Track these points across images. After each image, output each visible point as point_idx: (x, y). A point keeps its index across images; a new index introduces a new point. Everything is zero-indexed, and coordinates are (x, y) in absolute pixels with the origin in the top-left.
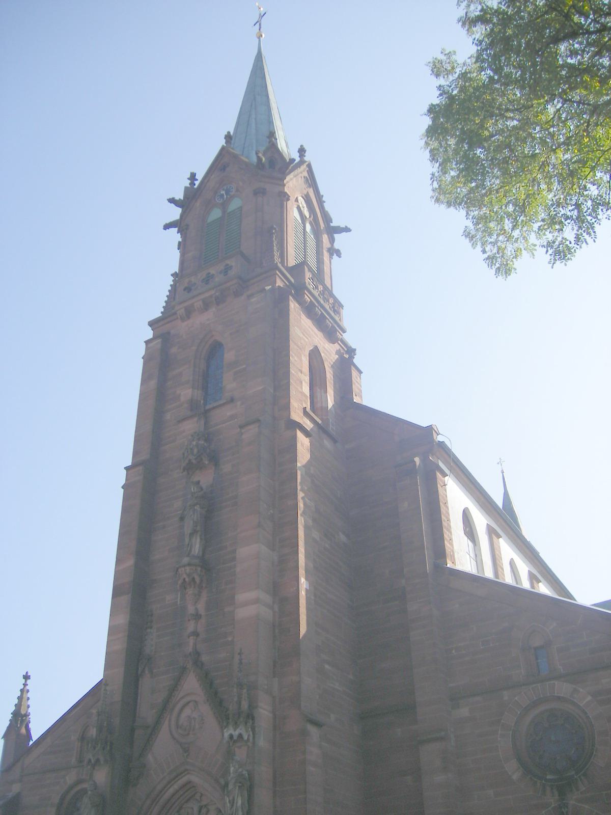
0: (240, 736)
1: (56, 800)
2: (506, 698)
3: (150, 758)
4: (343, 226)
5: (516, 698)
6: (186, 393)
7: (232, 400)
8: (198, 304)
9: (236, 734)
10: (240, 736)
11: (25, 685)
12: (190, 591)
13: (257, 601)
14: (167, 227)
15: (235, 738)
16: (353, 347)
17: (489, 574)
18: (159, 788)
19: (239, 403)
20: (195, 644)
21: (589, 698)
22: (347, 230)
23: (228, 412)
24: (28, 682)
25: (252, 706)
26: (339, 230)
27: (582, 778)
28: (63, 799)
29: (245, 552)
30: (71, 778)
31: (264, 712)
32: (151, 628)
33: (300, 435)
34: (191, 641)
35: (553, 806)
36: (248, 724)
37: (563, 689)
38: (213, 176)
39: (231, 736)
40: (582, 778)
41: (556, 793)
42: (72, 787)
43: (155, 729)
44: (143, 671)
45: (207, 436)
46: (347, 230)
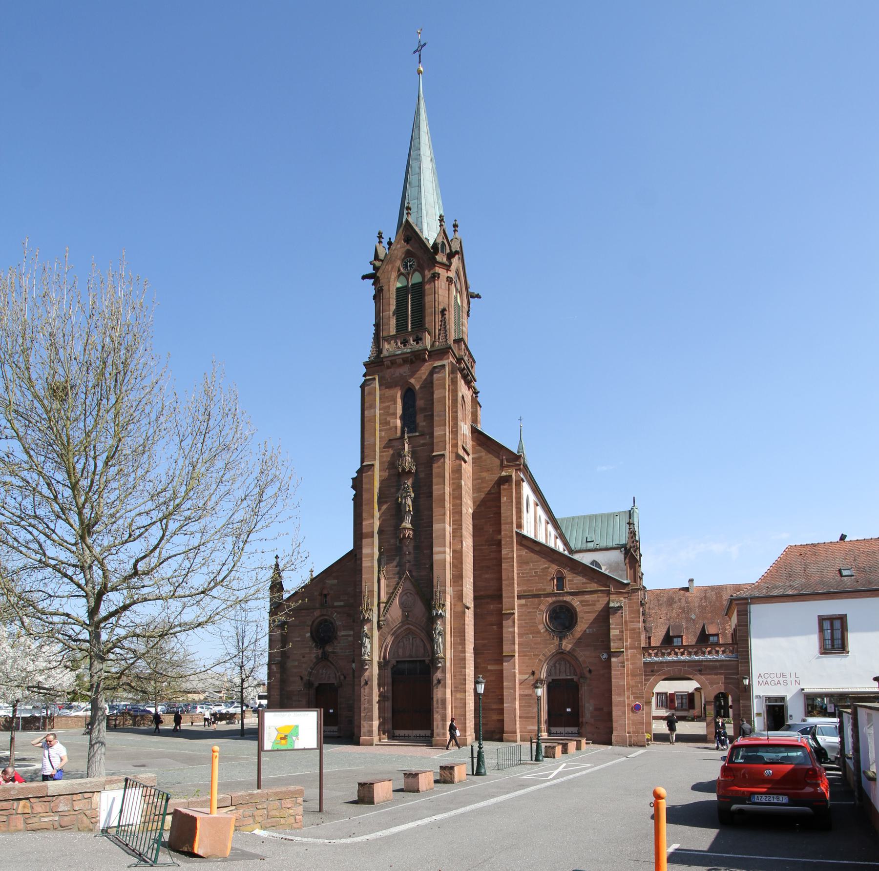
1: (310, 623)
30: (317, 613)
37: (568, 598)
42: (317, 618)
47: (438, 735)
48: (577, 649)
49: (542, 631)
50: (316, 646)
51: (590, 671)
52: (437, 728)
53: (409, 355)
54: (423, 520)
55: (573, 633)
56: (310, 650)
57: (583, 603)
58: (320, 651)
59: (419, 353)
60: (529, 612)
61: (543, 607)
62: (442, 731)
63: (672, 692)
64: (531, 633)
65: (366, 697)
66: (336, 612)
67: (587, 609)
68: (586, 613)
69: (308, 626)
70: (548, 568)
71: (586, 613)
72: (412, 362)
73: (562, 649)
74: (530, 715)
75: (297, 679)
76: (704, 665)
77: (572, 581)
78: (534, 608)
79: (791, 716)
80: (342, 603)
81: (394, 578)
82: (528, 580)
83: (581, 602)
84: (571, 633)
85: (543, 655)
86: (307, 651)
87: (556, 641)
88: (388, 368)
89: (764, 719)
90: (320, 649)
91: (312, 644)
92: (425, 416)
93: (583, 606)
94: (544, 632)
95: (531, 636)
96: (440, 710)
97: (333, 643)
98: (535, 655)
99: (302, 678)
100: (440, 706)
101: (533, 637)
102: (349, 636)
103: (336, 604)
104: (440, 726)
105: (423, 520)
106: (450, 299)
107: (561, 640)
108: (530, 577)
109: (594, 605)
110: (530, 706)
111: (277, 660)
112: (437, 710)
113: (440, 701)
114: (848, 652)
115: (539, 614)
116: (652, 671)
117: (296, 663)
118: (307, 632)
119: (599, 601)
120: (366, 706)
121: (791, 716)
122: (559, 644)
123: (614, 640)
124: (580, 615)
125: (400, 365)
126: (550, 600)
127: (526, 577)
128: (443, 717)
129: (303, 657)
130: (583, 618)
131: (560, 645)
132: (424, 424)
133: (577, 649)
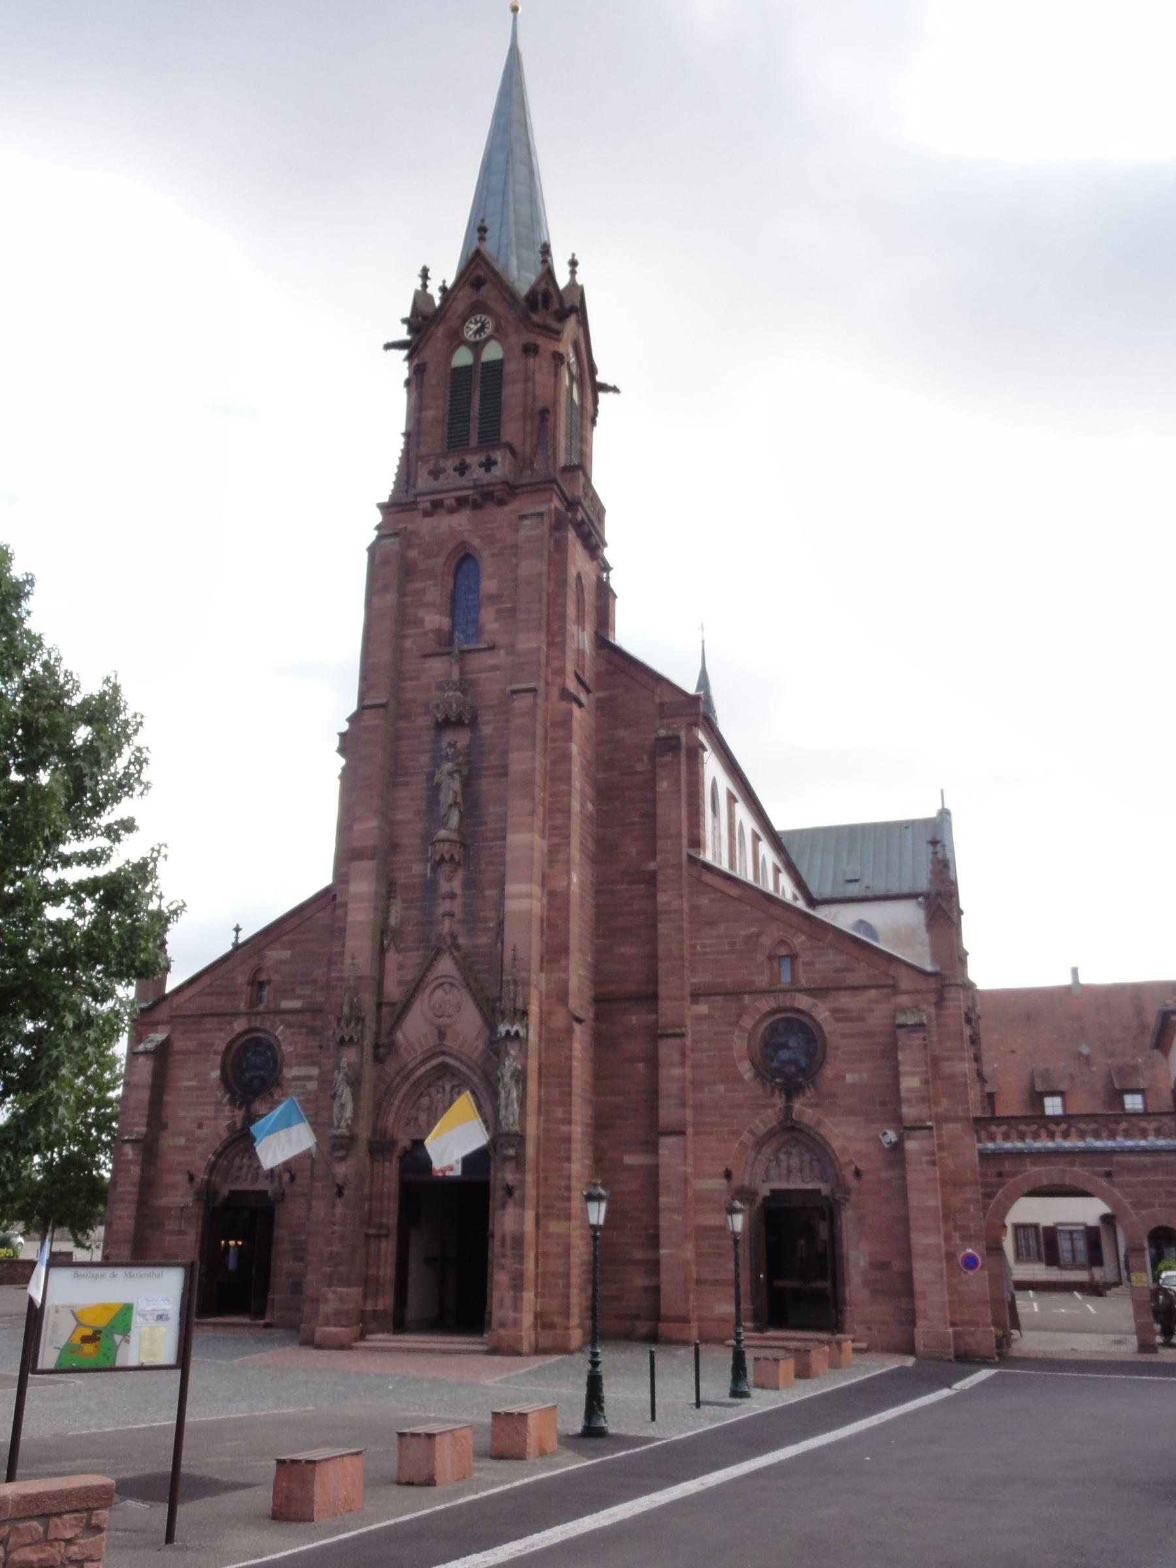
0: (517, 1033)
2: (746, 1002)
3: (399, 1036)
4: (611, 384)
5: (972, 1224)
6: (435, 620)
7: (492, 648)
8: (449, 501)
9: (513, 1031)
10: (517, 1033)
12: (446, 868)
13: (530, 895)
14: (388, 346)
15: (512, 1034)
16: (611, 565)
17: (749, 878)
18: (411, 1066)
19: (502, 652)
20: (451, 926)
21: (827, 1014)
22: (615, 390)
23: (489, 660)
24: (240, 933)
25: (527, 1003)
26: (605, 388)
27: (810, 1086)
28: (230, 1045)
29: (516, 839)
30: (240, 1025)
31: (534, 1009)
32: (395, 898)
33: (575, 707)
34: (447, 922)
35: (779, 1106)
36: (63, 791)
37: (803, 1002)
38: (461, 294)
39: (508, 1033)
42: (240, 1035)
43: (406, 1006)
44: (389, 945)
45: (466, 686)
46: (615, 390)
47: (503, 1325)
48: (826, 1120)
50: (232, 1102)
51: (858, 1174)
52: (501, 1306)
53: (470, 492)
54: (486, 824)
56: (217, 1111)
57: (839, 1015)
58: (240, 1114)
59: (491, 488)
61: (748, 1022)
62: (512, 1315)
65: (336, 1228)
66: (283, 1022)
67: (847, 1027)
68: (844, 1036)
69: (216, 1053)
70: (758, 935)
71: (844, 1036)
72: (476, 506)
74: (719, 1277)
75: (181, 1179)
77: (812, 964)
80: (297, 1004)
81: (417, 949)
83: (833, 1011)
85: (752, 1132)
86: (210, 1111)
87: (779, 1101)
88: (427, 514)
90: (240, 1108)
91: (223, 1096)
92: (498, 611)
93: (838, 1020)
95: (722, 1088)
96: (508, 1262)
97: (271, 1095)
99: (191, 1178)
100: (508, 1252)
102: (309, 1078)
103: (286, 1004)
104: (508, 1301)
105: (486, 824)
111: (138, 1133)
112: (502, 1261)
113: (509, 1240)
117: (182, 1141)
118: (213, 1068)
119: (872, 1010)
120: (335, 1249)
121: (147, 786)
123: (909, 1100)
124: (832, 1041)
125: (452, 511)
128: (514, 1279)
129: (200, 1126)
130: (837, 1048)
131: (788, 1110)
132: (496, 626)
133: (826, 1120)
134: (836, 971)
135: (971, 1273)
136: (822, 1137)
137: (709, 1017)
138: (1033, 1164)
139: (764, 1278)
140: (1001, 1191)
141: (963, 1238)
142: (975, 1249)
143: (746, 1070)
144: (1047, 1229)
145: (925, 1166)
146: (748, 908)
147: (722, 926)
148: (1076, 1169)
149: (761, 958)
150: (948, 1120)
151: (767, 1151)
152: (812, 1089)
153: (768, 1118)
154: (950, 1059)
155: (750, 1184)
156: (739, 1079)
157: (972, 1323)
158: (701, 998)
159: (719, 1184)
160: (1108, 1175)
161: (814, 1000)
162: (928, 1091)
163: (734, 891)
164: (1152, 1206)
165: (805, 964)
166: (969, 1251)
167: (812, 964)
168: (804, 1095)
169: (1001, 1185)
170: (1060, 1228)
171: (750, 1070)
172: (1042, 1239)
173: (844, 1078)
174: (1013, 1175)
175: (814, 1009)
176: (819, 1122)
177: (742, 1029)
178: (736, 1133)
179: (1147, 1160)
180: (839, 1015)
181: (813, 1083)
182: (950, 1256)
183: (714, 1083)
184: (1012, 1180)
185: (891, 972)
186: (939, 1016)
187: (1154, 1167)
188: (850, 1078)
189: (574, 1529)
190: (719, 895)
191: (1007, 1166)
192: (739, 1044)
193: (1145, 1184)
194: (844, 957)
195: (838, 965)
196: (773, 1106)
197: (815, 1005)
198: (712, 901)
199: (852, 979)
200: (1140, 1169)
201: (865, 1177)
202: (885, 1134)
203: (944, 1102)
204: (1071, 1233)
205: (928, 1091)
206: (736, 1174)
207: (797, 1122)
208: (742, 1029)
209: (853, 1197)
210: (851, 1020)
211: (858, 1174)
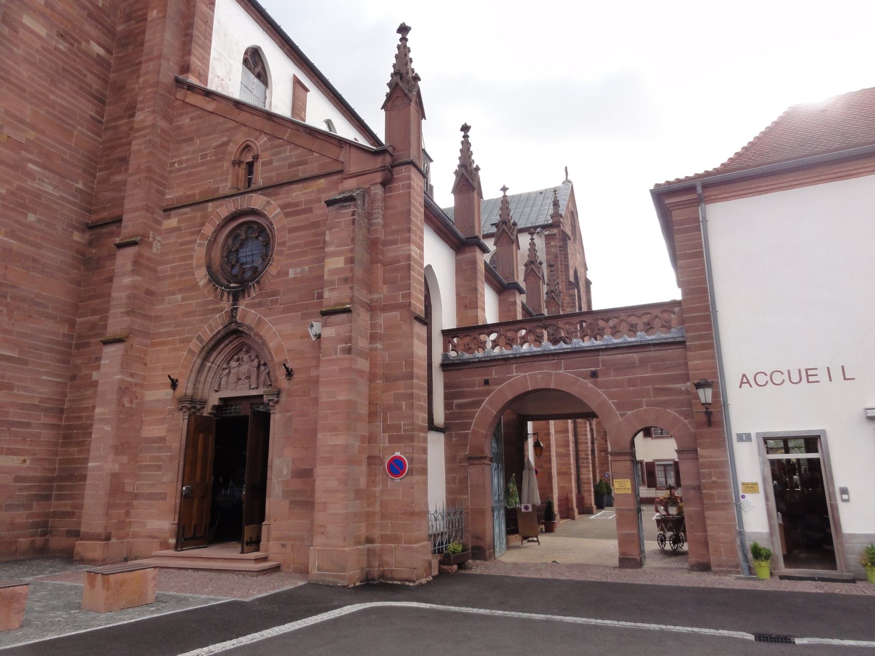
11: (466, 137)
27: (255, 285)
37: (257, 201)
40: (255, 285)
41: (231, 298)
48: (266, 319)
49: (201, 284)
51: (289, 373)
55: (262, 280)
57: (289, 210)
60: (182, 244)
61: (209, 230)
63: (650, 460)
64: (181, 291)
67: (294, 222)
68: (291, 230)
71: (291, 230)
73: (236, 322)
74: (154, 490)
76: (603, 361)
77: (270, 163)
78: (192, 234)
79: (844, 491)
82: (190, 175)
83: (283, 207)
84: (258, 282)
85: (199, 338)
87: (226, 304)
89: (767, 499)
93: (287, 215)
94: (205, 286)
95: (179, 297)
98: (182, 341)
101: (183, 299)
106: (816, 577)
107: (236, 300)
108: (193, 167)
109: (309, 210)
110: (159, 467)
114: (824, 431)
115: (200, 245)
116: (486, 382)
121: (844, 491)
122: (232, 310)
123: (332, 283)
126: (225, 209)
127: (186, 168)
133: (266, 319)
134: (291, 166)
135: (397, 480)
136: (261, 337)
137: (178, 229)
138: (518, 370)
139: (246, 495)
140: (487, 399)
141: (391, 440)
142: (404, 453)
143: (201, 276)
144: (647, 464)
145: (339, 356)
146: (221, 120)
147: (198, 141)
148: (562, 371)
149: (227, 165)
150: (385, 309)
151: (218, 358)
152: (257, 289)
153: (216, 323)
154: (395, 242)
155: (194, 394)
156: (195, 287)
157: (395, 539)
158: (173, 212)
159: (166, 393)
160: (594, 375)
161: (268, 199)
162: (352, 270)
163: (211, 106)
164: (639, 405)
165: (264, 164)
166: (398, 454)
167: (270, 163)
168: (249, 296)
169: (488, 393)
170: (657, 463)
171: (206, 275)
172: (645, 471)
173: (287, 274)
174: (498, 382)
175: (267, 208)
176: (260, 322)
177: (203, 237)
178: (188, 341)
179: (635, 356)
180: (289, 210)
181: (258, 282)
182: (372, 460)
183: (174, 294)
184: (498, 387)
185: (341, 159)
186: (385, 199)
187: (643, 362)
188: (292, 273)
189: (817, 587)
190: (200, 112)
191: (494, 373)
192: (199, 252)
193: (632, 383)
194: (299, 151)
195: (293, 160)
196: (222, 309)
197: (268, 203)
198: (192, 119)
199: (303, 172)
200: (631, 366)
201: (296, 376)
202: (312, 326)
203: (385, 289)
204: (665, 466)
205: (352, 270)
206: (181, 384)
207: (241, 325)
208: (203, 237)
209: (283, 398)
210: (298, 213)
211: (289, 373)
